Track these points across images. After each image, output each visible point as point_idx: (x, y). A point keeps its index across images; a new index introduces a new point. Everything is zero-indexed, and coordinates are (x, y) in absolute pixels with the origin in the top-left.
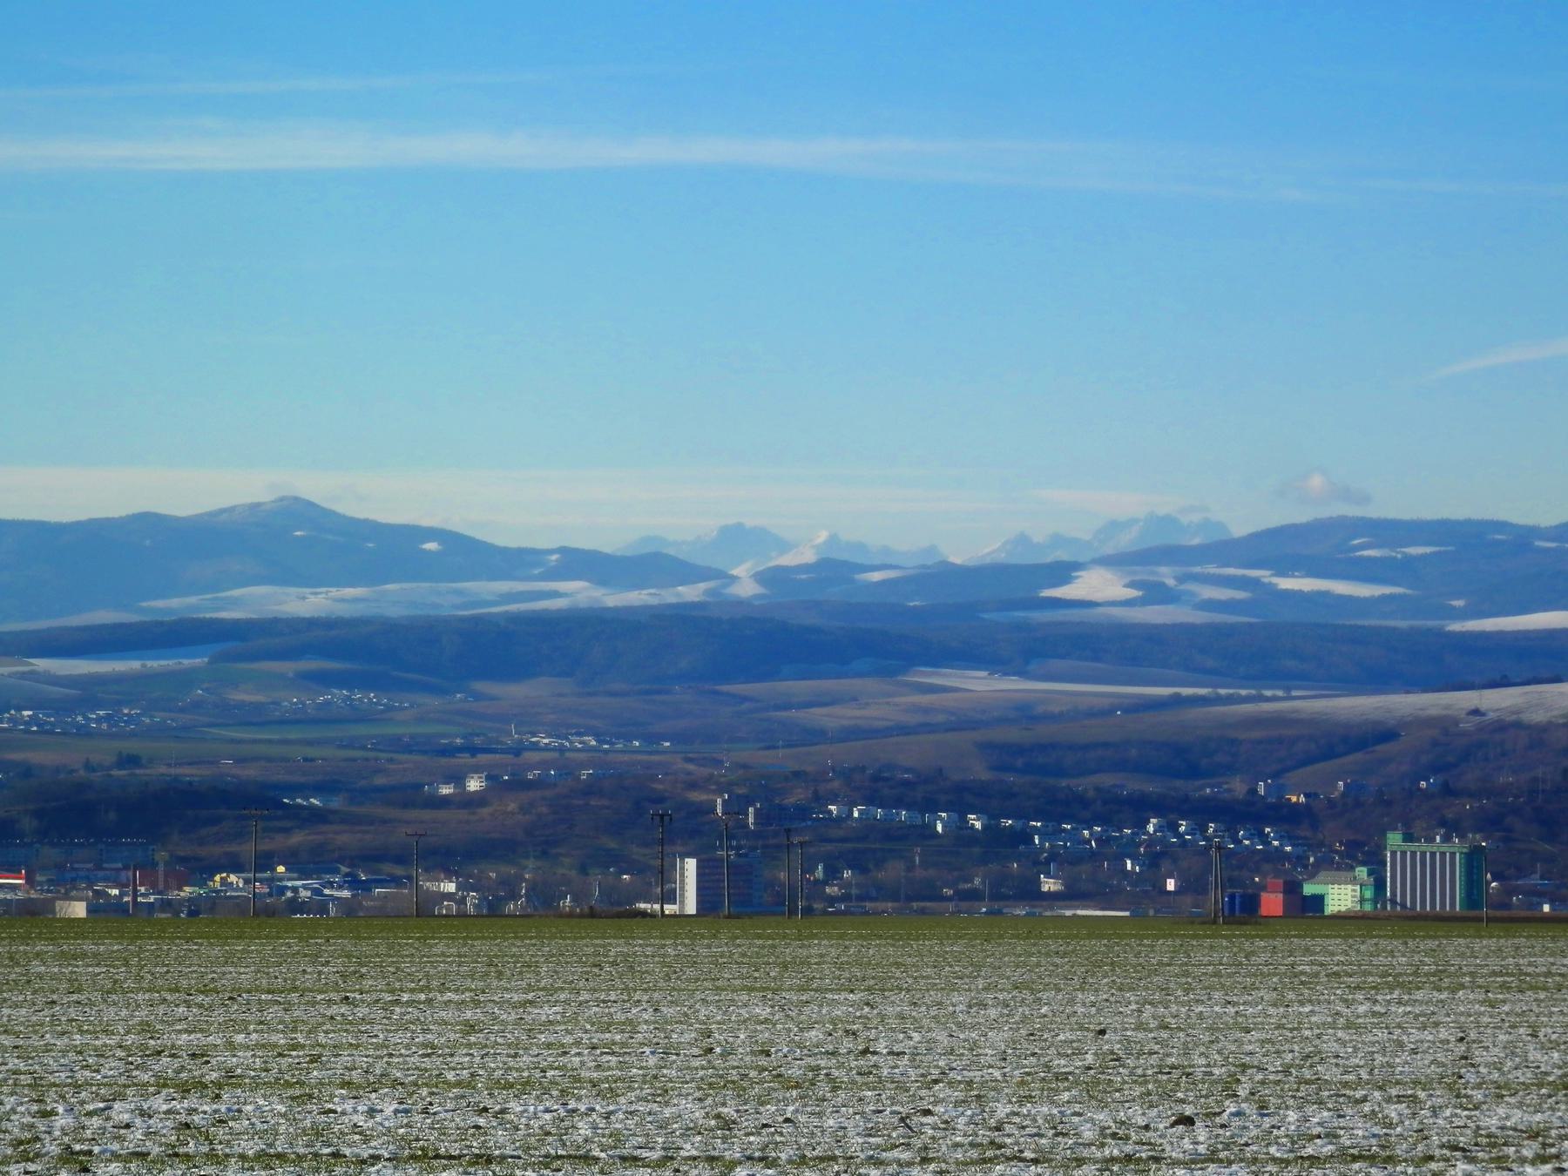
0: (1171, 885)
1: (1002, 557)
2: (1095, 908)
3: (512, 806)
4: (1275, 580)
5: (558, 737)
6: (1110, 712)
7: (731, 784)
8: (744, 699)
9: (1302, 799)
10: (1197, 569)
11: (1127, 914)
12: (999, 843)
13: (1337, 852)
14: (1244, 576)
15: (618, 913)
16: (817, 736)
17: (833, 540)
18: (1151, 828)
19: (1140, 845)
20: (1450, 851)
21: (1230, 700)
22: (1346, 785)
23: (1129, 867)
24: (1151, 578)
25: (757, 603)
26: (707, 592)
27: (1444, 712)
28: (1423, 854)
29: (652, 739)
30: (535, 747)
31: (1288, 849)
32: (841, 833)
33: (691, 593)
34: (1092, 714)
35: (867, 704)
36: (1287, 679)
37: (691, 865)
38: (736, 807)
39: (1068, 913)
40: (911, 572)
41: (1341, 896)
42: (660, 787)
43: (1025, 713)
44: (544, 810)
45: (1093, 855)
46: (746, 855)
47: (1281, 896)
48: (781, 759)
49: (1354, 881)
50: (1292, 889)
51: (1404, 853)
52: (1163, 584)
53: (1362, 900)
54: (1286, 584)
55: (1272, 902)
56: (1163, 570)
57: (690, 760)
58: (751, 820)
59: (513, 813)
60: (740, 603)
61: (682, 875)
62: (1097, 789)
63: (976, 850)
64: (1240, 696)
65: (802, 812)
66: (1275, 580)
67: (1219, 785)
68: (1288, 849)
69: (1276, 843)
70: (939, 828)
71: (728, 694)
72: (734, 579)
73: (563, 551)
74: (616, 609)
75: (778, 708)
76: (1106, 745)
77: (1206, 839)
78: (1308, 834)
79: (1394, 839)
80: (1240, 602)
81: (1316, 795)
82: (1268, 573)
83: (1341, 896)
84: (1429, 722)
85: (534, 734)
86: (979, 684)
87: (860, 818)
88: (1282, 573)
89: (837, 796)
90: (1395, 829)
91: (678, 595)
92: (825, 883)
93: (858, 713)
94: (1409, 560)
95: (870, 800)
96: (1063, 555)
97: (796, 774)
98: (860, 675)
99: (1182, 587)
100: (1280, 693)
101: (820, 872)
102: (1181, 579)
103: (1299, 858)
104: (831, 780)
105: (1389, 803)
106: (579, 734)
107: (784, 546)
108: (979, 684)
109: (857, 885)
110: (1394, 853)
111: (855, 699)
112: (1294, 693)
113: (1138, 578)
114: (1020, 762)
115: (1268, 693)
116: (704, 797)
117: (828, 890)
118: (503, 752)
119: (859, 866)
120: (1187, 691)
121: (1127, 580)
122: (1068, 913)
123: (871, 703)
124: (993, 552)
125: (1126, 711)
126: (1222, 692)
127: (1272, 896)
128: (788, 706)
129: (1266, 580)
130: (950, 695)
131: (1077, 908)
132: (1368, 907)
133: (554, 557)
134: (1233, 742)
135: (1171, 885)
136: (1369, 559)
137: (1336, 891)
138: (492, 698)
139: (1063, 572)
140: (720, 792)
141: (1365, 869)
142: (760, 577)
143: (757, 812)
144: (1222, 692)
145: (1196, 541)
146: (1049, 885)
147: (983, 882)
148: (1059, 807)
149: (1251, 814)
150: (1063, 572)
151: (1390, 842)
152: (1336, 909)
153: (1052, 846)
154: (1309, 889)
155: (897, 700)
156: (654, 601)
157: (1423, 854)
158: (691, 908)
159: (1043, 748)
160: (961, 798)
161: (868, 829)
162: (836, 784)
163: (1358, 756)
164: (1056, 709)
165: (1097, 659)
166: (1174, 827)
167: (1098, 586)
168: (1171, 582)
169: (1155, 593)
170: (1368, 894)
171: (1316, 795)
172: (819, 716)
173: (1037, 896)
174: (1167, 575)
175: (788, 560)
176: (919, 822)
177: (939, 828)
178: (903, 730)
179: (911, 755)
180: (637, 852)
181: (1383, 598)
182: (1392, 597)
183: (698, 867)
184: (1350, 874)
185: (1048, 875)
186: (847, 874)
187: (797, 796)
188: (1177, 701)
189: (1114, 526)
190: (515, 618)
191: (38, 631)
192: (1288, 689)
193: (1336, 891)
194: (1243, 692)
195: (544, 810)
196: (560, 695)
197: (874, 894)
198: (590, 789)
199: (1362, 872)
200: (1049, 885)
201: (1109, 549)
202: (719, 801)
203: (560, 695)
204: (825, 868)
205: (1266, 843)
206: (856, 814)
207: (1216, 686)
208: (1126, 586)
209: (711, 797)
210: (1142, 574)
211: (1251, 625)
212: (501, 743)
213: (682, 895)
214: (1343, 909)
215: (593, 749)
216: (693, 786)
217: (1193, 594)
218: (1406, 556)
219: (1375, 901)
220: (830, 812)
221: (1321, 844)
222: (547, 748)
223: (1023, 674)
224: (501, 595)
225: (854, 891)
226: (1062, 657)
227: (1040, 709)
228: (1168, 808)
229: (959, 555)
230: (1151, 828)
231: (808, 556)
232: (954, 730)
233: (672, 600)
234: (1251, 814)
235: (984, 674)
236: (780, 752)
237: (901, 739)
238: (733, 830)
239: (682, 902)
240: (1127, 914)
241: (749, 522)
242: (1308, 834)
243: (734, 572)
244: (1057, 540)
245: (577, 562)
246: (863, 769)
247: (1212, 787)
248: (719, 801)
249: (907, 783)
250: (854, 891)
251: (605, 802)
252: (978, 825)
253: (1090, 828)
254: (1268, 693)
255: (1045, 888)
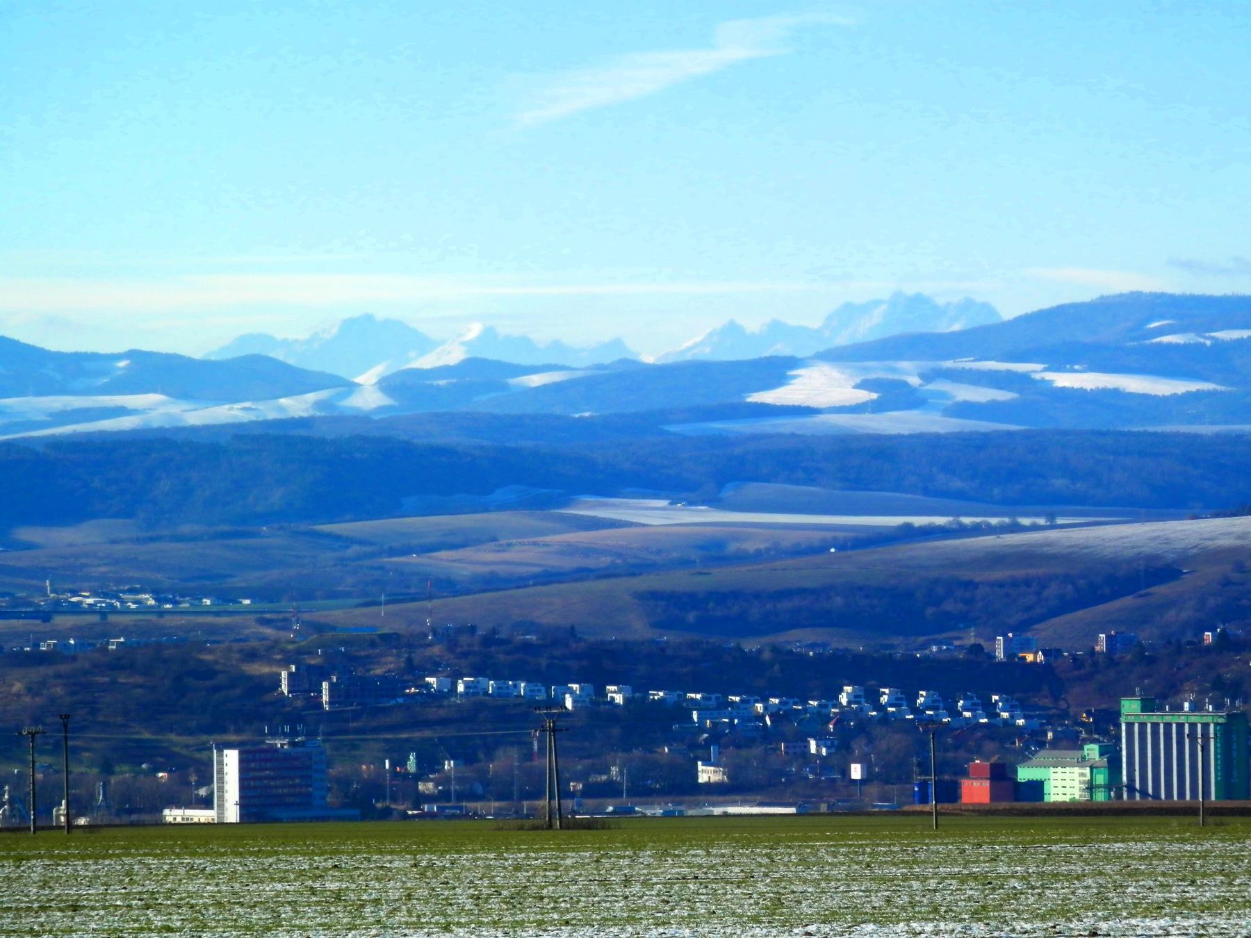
0: (856, 772)
1: (707, 354)
2: (744, 803)
3: (18, 687)
4: (1049, 376)
5: (106, 595)
6: (822, 549)
7: (299, 652)
8: (349, 541)
9: (1040, 657)
10: (948, 364)
11: (792, 810)
12: (642, 724)
13: (1083, 724)
14: (1008, 372)
15: (133, 818)
16: (448, 586)
17: (489, 334)
18: (844, 699)
19: (828, 720)
20: (1197, 716)
21: (976, 530)
22: (1109, 638)
23: (813, 749)
24: (891, 376)
25: (376, 417)
26: (319, 405)
27: (1239, 542)
28: (1168, 726)
29: (226, 596)
30: (76, 609)
31: (1021, 722)
32: (442, 713)
33: (296, 406)
34: (797, 551)
35: (509, 545)
36: (1056, 505)
37: (231, 758)
38: (306, 681)
39: (718, 811)
40: (579, 374)
41: (1064, 782)
42: (208, 657)
43: (713, 550)
44: (59, 691)
45: (767, 736)
46: (302, 744)
47: (987, 784)
48: (385, 618)
49: (1082, 762)
50: (1001, 775)
51: (1143, 726)
52: (905, 384)
53: (1091, 787)
54: (1063, 380)
55: (976, 790)
56: (905, 365)
57: (267, 622)
58: (325, 698)
59: (18, 695)
60: (362, 418)
61: (221, 771)
62: (775, 650)
63: (616, 731)
64: (989, 525)
65: (392, 686)
66: (1049, 376)
67: (948, 642)
68: (1021, 722)
69: (1005, 715)
70: (569, 703)
71: (329, 536)
72: (351, 387)
73: (131, 354)
74: (194, 429)
75: (393, 552)
76: (802, 592)
77: (914, 710)
78: (1047, 702)
79: (1130, 708)
80: (1004, 403)
81: (1058, 652)
82: (1039, 367)
83: (1064, 782)
84: (1214, 556)
85: (75, 593)
86: (656, 517)
87: (466, 693)
88: (1059, 369)
89: (437, 664)
90: (1133, 695)
91: (281, 409)
92: (420, 776)
93: (491, 557)
94: (1221, 348)
95: (478, 671)
96: (781, 349)
97: (385, 637)
98: (502, 507)
99: (929, 387)
100: (1041, 521)
101: (412, 764)
102: (927, 377)
103: (1033, 733)
104: (430, 645)
105: (1152, 661)
106: (132, 591)
107: (426, 344)
108: (656, 517)
109: (460, 780)
110: (1130, 726)
111: (494, 539)
112: (1060, 521)
113: (873, 376)
114: (691, 617)
115: (1025, 521)
116: (266, 670)
117: (421, 787)
118: (29, 616)
119: (466, 756)
120: (919, 521)
121: (858, 380)
122: (718, 811)
123: (509, 546)
124: (696, 345)
125: (841, 548)
126: (967, 520)
127: (976, 784)
128: (406, 551)
129: (1037, 376)
130: (633, 530)
131: (734, 803)
132: (1100, 797)
133: (122, 364)
134: (970, 585)
135: (856, 772)
136: (1170, 346)
137: (1060, 776)
138: (30, 546)
139: (777, 370)
140: (285, 663)
141: (1095, 747)
142: (386, 385)
143: (332, 687)
144: (967, 520)
145: (956, 327)
146: (707, 774)
147: (621, 773)
148: (725, 672)
149: (977, 675)
150: (777, 370)
151: (1124, 711)
152: (1060, 798)
153: (714, 724)
154: (1025, 774)
155: (548, 539)
156: (245, 417)
157: (1168, 726)
158: (232, 814)
159: (721, 597)
160: (598, 664)
161: (477, 707)
162: (436, 650)
163: (1128, 601)
164: (751, 547)
165: (810, 481)
166: (873, 697)
167: (822, 389)
168: (914, 381)
169: (894, 395)
170: (1101, 779)
171: (1058, 652)
172: (446, 562)
173: (688, 788)
174: (909, 372)
175: (427, 362)
176: (541, 696)
177: (569, 703)
178: (549, 577)
179: (552, 608)
180: (176, 740)
181: (1189, 396)
182: (1197, 396)
183: (241, 761)
184: (1078, 754)
185: (707, 762)
186: (449, 765)
187: (386, 665)
188: (908, 534)
189: (849, 312)
190: (56, 444)
191: (120, 433)
192: (1051, 516)
193: (1060, 776)
194: (994, 521)
195: (59, 691)
196: (114, 542)
197: (479, 789)
198: (119, 663)
199: (1092, 751)
200: (707, 774)
201: (843, 339)
202: (284, 674)
203: (114, 542)
204: (417, 758)
205: (993, 715)
206: (461, 688)
207: (959, 515)
208: (857, 387)
209: (275, 669)
210: (878, 371)
211: (1009, 434)
212: (29, 604)
213: (221, 798)
214: (1067, 799)
215: (149, 610)
216: (252, 656)
217: (943, 395)
218: (1217, 343)
219: (1108, 787)
220: (428, 686)
221: (1064, 714)
222: (92, 610)
223: (715, 502)
224: (51, 415)
225: (454, 787)
226: (767, 479)
227: (732, 548)
228: (867, 673)
229: (651, 352)
230: (844, 699)
231: (454, 356)
232: (607, 576)
233: (272, 415)
234: (977, 675)
235: (663, 503)
236: (383, 610)
237: (540, 588)
238: (300, 715)
239: (221, 807)
240: (792, 810)
241: (380, 315)
242: (1047, 702)
243: (357, 380)
244: (776, 328)
245: (153, 370)
246: (473, 629)
247: (939, 643)
248: (284, 674)
249: (527, 646)
250: (454, 787)
251: (139, 680)
252: (619, 699)
253: (764, 700)
254: (1025, 521)
255: (703, 778)
